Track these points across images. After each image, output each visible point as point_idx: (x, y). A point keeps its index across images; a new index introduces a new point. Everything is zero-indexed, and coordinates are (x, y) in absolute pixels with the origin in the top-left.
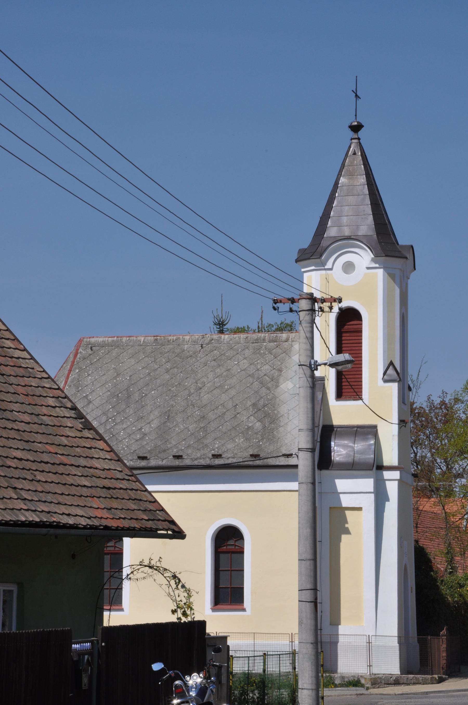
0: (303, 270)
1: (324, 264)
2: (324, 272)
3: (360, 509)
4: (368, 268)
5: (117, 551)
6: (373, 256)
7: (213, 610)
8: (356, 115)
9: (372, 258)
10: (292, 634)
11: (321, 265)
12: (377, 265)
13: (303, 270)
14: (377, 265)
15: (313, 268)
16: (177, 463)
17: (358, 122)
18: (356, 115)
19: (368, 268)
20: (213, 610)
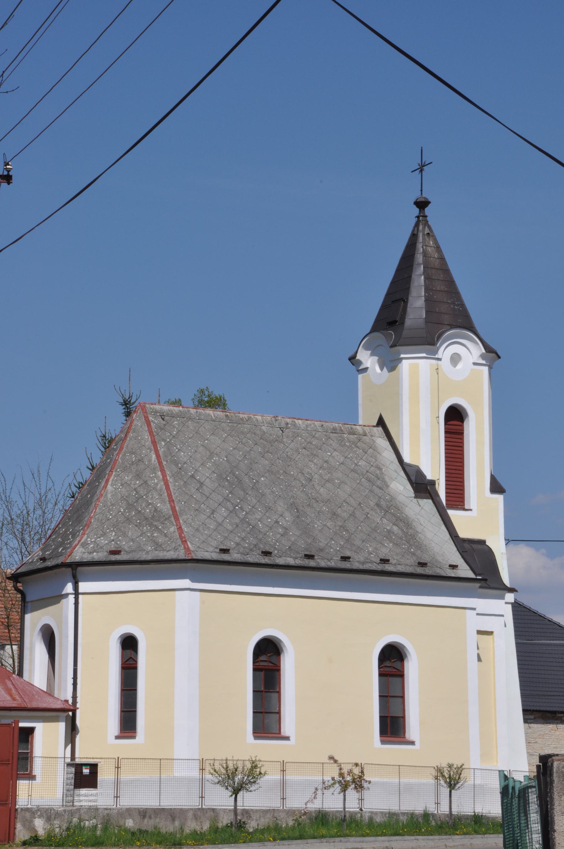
0: (402, 356)
1: (436, 352)
2: (434, 362)
3: (491, 633)
4: (475, 364)
5: (271, 668)
6: (484, 351)
7: (256, 738)
8: (421, 191)
9: (483, 353)
10: (118, 758)
11: (433, 354)
12: (484, 362)
13: (402, 356)
14: (484, 362)
15: (424, 355)
16: (420, 570)
17: (425, 198)
18: (421, 191)
19: (475, 364)
20: (383, 742)
